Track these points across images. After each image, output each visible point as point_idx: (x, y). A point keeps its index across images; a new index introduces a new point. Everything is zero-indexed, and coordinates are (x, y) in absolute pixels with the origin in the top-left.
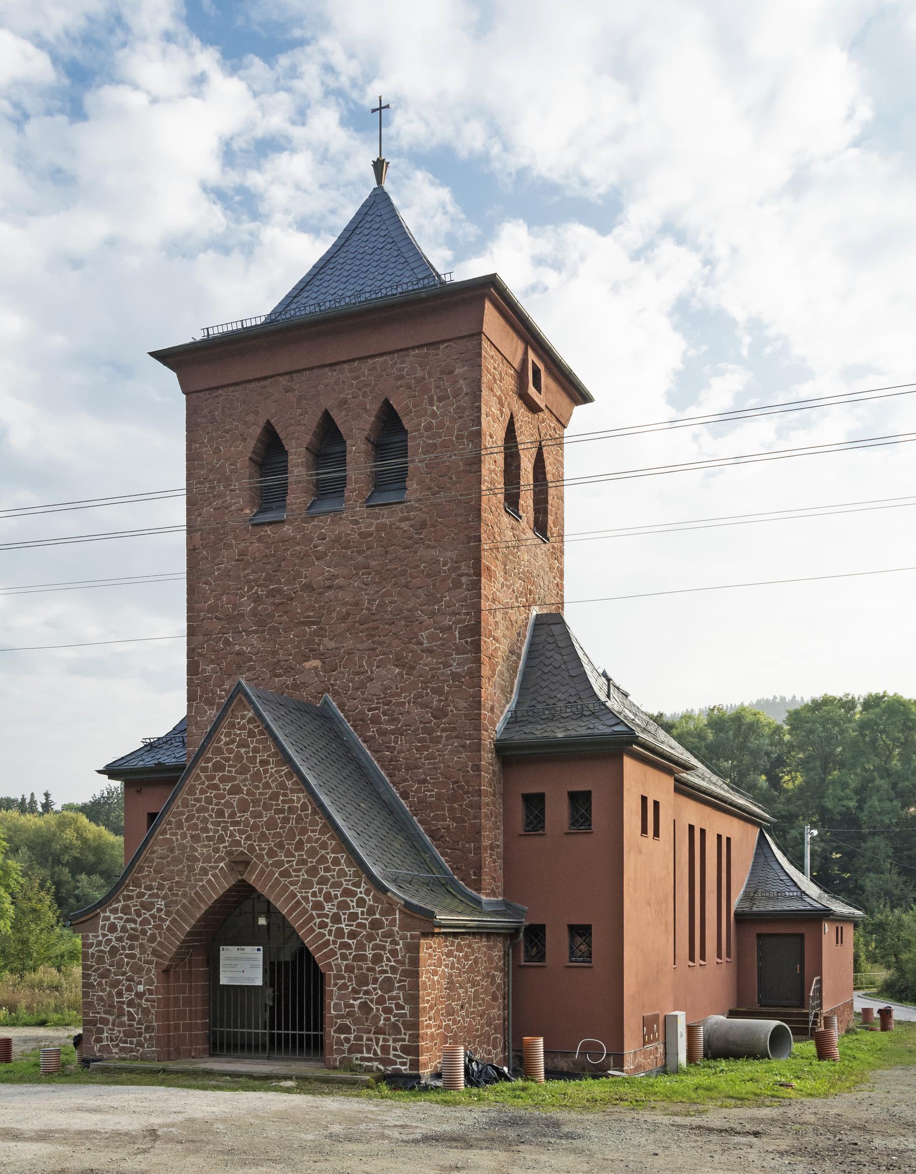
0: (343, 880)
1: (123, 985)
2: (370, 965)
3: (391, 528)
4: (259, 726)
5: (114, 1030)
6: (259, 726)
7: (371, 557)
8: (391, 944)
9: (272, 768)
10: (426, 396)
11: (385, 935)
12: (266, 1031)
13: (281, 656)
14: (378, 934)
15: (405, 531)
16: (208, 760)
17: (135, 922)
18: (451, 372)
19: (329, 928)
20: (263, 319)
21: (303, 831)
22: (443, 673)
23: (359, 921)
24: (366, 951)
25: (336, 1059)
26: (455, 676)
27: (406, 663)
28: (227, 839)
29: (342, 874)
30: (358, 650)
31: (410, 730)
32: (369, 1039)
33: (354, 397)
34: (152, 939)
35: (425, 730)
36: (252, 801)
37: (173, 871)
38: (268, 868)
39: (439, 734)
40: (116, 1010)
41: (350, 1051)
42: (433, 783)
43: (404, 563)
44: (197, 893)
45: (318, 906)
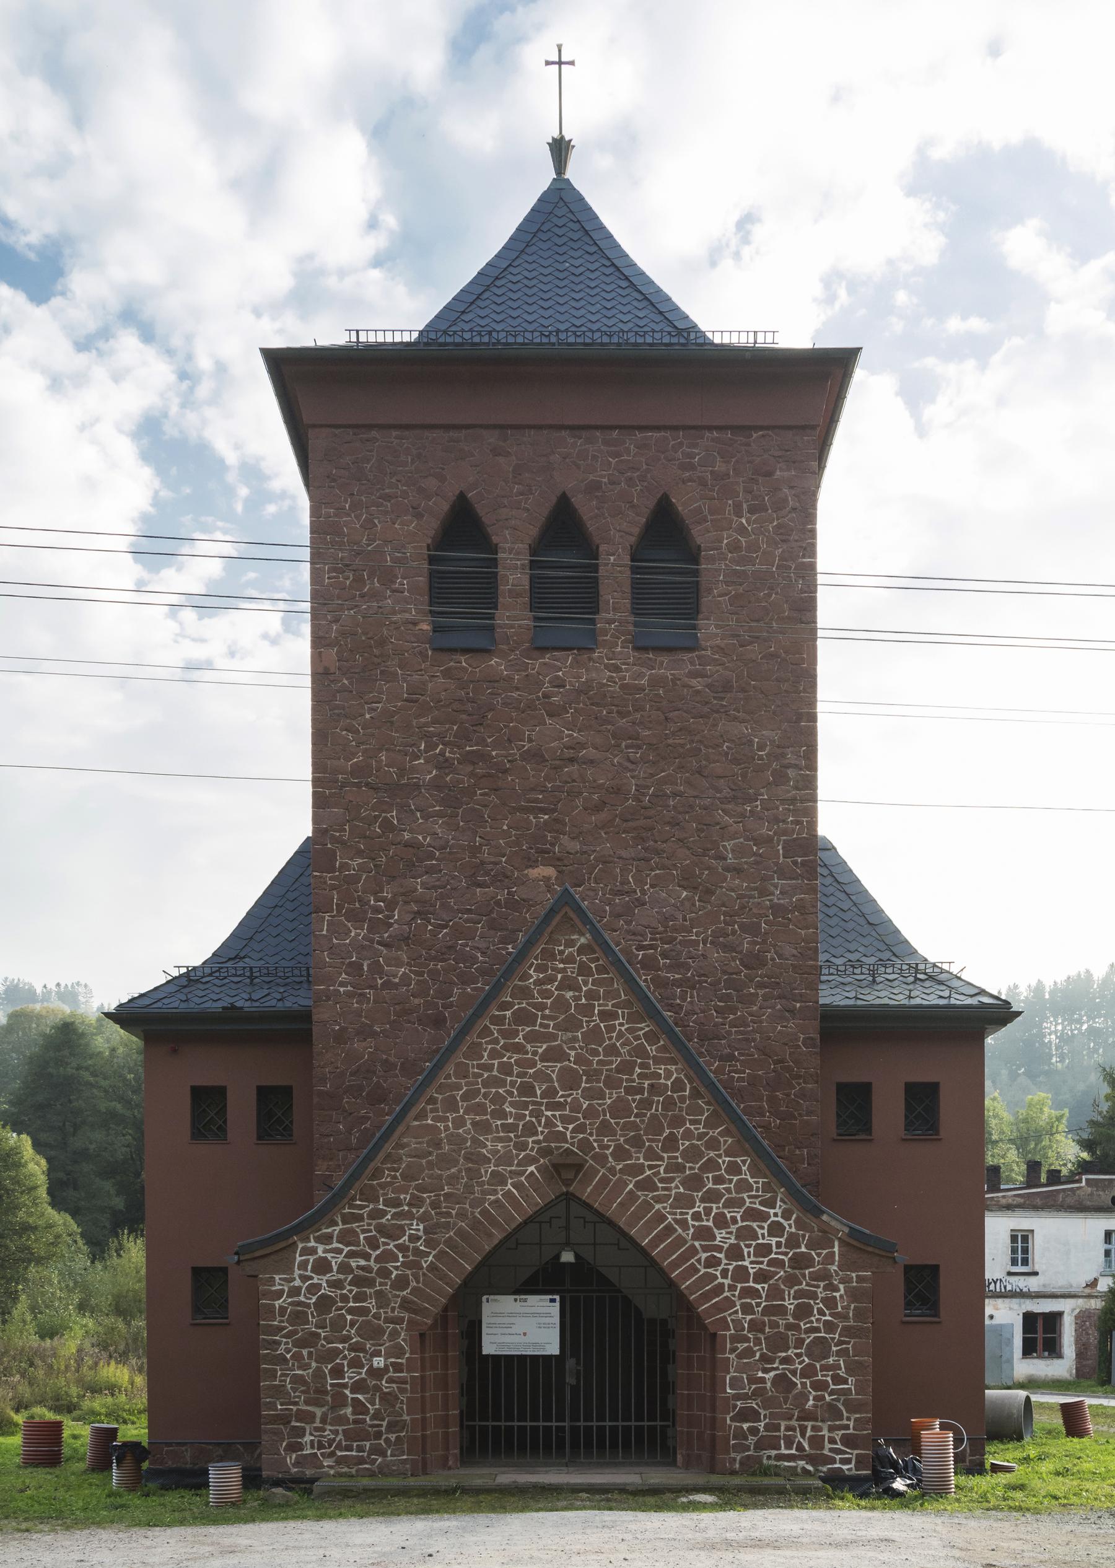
0: (745, 1196)
1: (345, 1357)
2: (791, 1320)
3: (675, 684)
4: (597, 959)
5: (325, 1431)
6: (597, 959)
7: (641, 723)
8: (825, 1288)
9: (621, 1025)
10: (730, 502)
11: (816, 1277)
12: (566, 1424)
13: (485, 854)
14: (804, 1276)
15: (698, 692)
16: (505, 1006)
17: (367, 1257)
18: (769, 474)
19: (722, 1266)
20: (415, 335)
21: (677, 1122)
22: (759, 903)
23: (773, 1256)
24: (784, 1300)
25: (734, 1460)
26: (776, 909)
27: (700, 884)
28: (540, 1129)
29: (742, 1186)
30: (619, 858)
31: (706, 982)
32: (788, 1429)
33: (612, 483)
34: (401, 1283)
35: (729, 984)
36: (585, 1072)
37: (440, 1177)
38: (614, 1176)
39: (753, 991)
40: (329, 1398)
41: (759, 1446)
42: (742, 1060)
43: (696, 738)
44: (484, 1213)
45: (704, 1234)
